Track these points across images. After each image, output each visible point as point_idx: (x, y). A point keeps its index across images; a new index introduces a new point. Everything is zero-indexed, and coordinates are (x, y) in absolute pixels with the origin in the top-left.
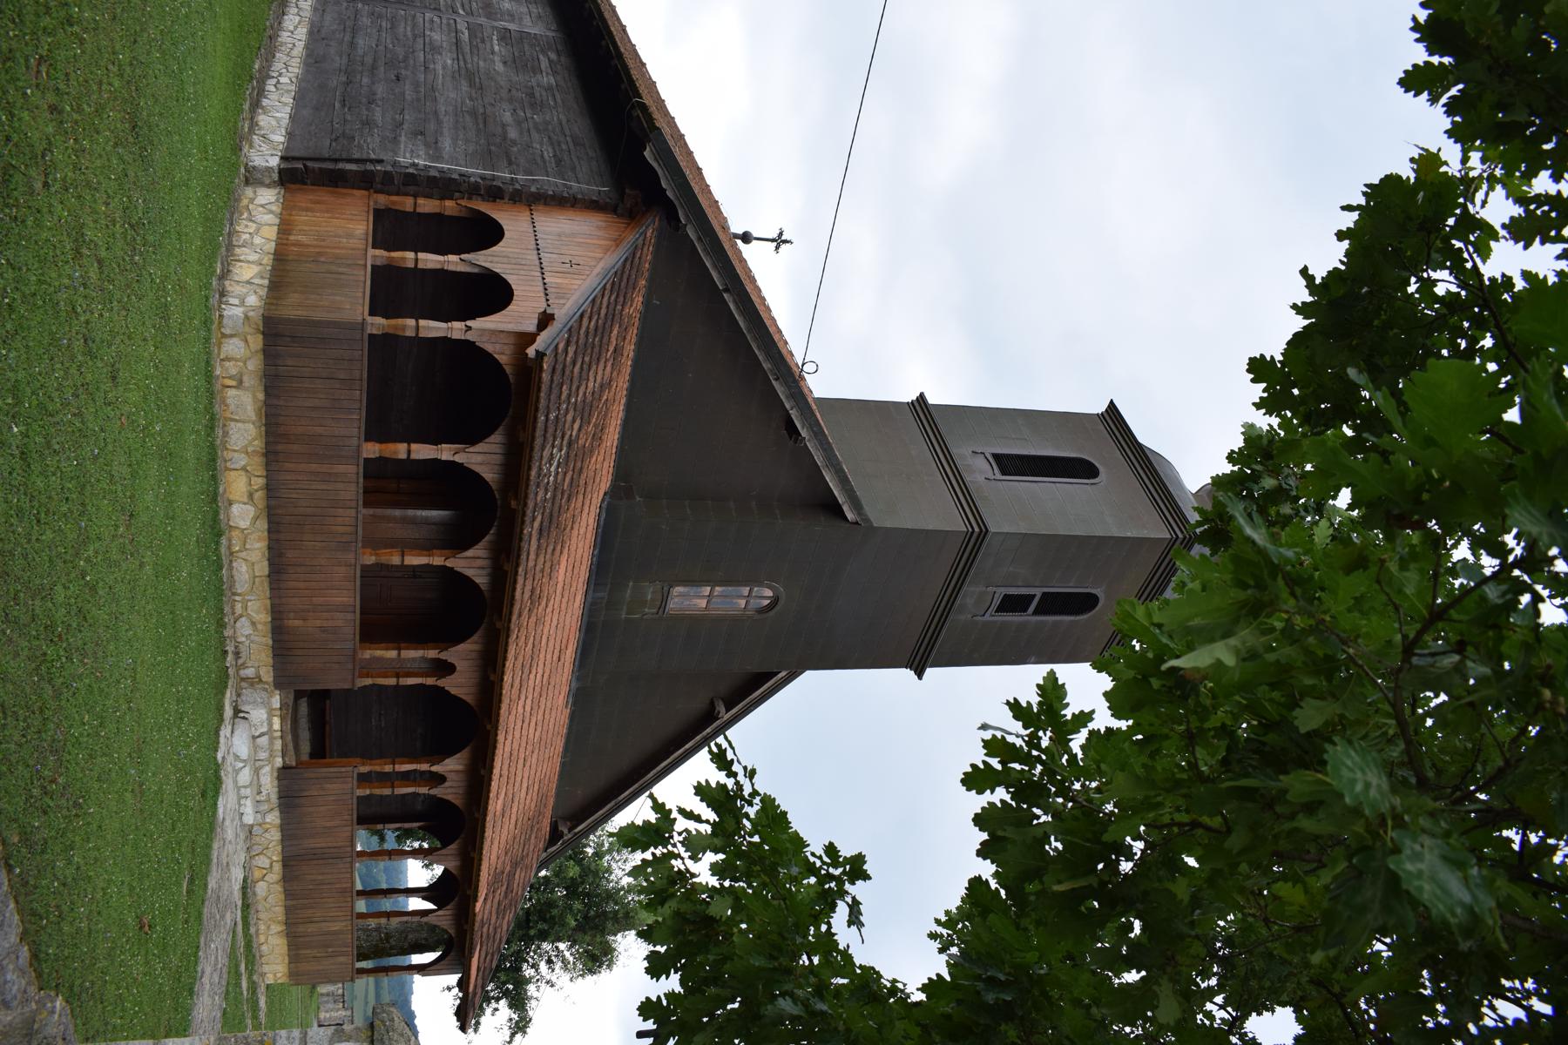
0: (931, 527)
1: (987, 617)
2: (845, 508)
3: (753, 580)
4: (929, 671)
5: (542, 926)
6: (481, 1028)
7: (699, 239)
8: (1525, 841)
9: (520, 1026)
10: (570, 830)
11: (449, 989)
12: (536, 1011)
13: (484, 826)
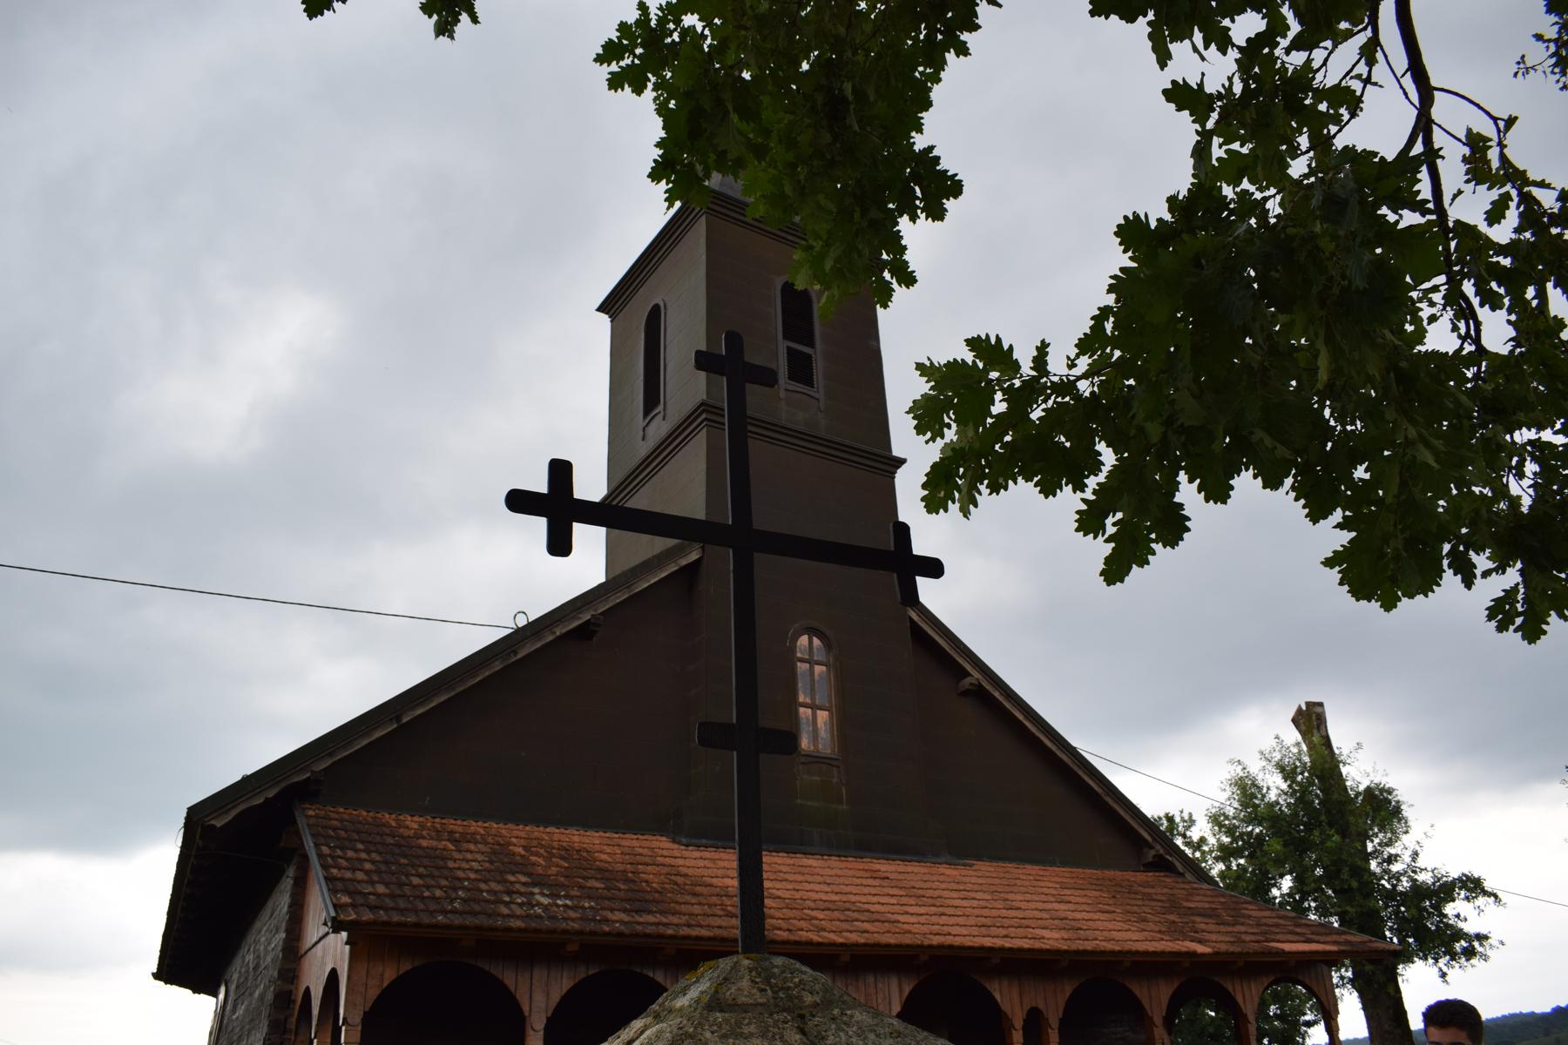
0: (704, 466)
1: (821, 396)
2: (684, 562)
4: (897, 451)
5: (1345, 875)
6: (1484, 931)
7: (331, 755)
9: (1473, 886)
10: (1151, 847)
11: (1443, 975)
13: (1077, 952)
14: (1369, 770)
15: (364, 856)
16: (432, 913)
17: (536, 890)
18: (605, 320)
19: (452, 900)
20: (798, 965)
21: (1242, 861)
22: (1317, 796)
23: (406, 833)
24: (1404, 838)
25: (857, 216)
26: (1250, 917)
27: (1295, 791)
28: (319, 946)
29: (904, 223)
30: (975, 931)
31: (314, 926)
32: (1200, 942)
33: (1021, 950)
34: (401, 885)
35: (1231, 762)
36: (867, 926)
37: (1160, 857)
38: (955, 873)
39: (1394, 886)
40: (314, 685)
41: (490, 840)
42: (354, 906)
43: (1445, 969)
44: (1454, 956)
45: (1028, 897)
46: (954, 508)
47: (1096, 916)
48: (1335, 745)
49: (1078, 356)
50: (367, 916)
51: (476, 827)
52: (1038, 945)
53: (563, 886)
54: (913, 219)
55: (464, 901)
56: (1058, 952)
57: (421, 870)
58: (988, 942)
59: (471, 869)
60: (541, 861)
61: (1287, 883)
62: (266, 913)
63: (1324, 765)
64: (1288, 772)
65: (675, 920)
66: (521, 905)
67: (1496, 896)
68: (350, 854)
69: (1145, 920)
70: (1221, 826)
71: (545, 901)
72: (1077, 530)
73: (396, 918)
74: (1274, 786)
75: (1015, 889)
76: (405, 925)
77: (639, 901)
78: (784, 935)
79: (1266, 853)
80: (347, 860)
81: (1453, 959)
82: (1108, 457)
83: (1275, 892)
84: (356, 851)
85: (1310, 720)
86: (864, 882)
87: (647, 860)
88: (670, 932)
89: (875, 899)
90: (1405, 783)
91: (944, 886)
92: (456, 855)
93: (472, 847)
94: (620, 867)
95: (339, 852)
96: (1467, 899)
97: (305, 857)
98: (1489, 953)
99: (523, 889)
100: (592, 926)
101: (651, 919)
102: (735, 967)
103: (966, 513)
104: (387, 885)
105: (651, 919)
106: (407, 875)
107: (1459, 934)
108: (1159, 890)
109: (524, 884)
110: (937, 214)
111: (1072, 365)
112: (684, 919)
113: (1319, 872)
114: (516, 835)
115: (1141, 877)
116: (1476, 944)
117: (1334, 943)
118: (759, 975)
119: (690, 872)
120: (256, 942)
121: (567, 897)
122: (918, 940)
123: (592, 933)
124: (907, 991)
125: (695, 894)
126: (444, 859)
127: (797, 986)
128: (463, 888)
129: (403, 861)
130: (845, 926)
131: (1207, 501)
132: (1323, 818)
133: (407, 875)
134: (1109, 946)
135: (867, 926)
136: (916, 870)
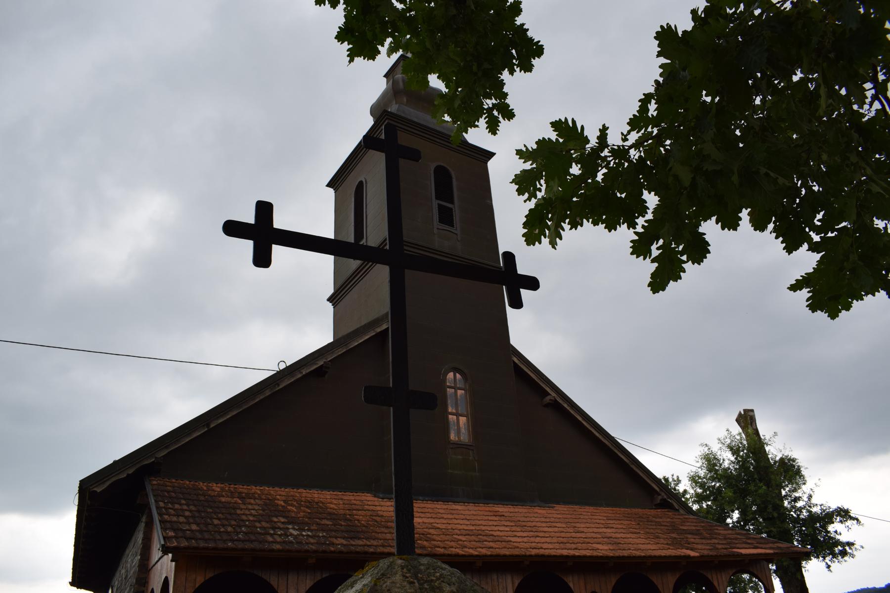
2: (379, 330)
3: (442, 385)
5: (770, 509)
6: (851, 540)
7: (167, 447)
8: (840, 89)
9: (844, 514)
10: (659, 495)
11: (829, 567)
12: (833, 505)
13: (619, 557)
14: (781, 448)
15: (185, 507)
16: (225, 541)
17: (290, 526)
18: (331, 191)
19: (238, 533)
20: (439, 563)
21: (709, 503)
22: (752, 464)
23: (213, 494)
24: (803, 487)
25: (475, 68)
26: (719, 534)
27: (739, 461)
28: (159, 563)
29: (505, 75)
30: (557, 546)
31: (156, 554)
32: (692, 549)
33: (585, 557)
34: (207, 525)
35: (702, 445)
36: (491, 544)
37: (664, 500)
38: (544, 512)
39: (798, 515)
40: (162, 406)
41: (263, 497)
42: (176, 537)
43: (829, 563)
44: (834, 556)
45: (588, 525)
46: (545, 241)
47: (628, 536)
48: (761, 434)
49: (629, 132)
50: (184, 543)
51: (256, 489)
52: (595, 554)
53: (307, 524)
54: (512, 72)
55: (246, 533)
56: (607, 557)
57: (220, 515)
58: (565, 552)
59: (251, 515)
60: (294, 509)
61: (736, 515)
62: (131, 545)
63: (755, 446)
64: (735, 451)
65: (375, 543)
66: (280, 535)
67: (857, 520)
68: (177, 506)
69: (658, 537)
70: (696, 482)
71: (295, 533)
72: (632, 254)
73: (202, 544)
74: (727, 458)
75: (580, 521)
76: (207, 548)
77: (353, 532)
78: (442, 551)
79: (723, 498)
80: (175, 510)
81: (834, 557)
82: (651, 200)
83: (729, 521)
84: (181, 505)
85: (746, 420)
86: (490, 518)
87: (357, 507)
88: (371, 550)
89: (496, 528)
90: (801, 456)
91: (537, 519)
92: (243, 506)
93: (252, 501)
94: (342, 512)
95: (170, 506)
96: (841, 522)
97: (150, 509)
98: (855, 553)
99: (282, 526)
100: (324, 547)
101: (360, 542)
102: (391, 566)
103: (553, 244)
104: (198, 525)
105: (360, 542)
106: (211, 519)
107: (838, 543)
108: (665, 520)
109: (283, 523)
110: (527, 67)
111: (625, 139)
112: (381, 542)
113: (754, 508)
114: (280, 494)
115: (653, 512)
116: (847, 548)
117: (771, 548)
118: (409, 571)
119: (385, 514)
120: (126, 562)
121: (308, 530)
122: (522, 552)
123: (324, 552)
124: (517, 583)
125: (387, 527)
126: (235, 509)
127: (438, 579)
128: (246, 526)
129: (209, 510)
130: (478, 544)
131: (723, 229)
132: (756, 476)
133: (211, 519)
134: (638, 553)
135: (491, 544)
136: (520, 510)
